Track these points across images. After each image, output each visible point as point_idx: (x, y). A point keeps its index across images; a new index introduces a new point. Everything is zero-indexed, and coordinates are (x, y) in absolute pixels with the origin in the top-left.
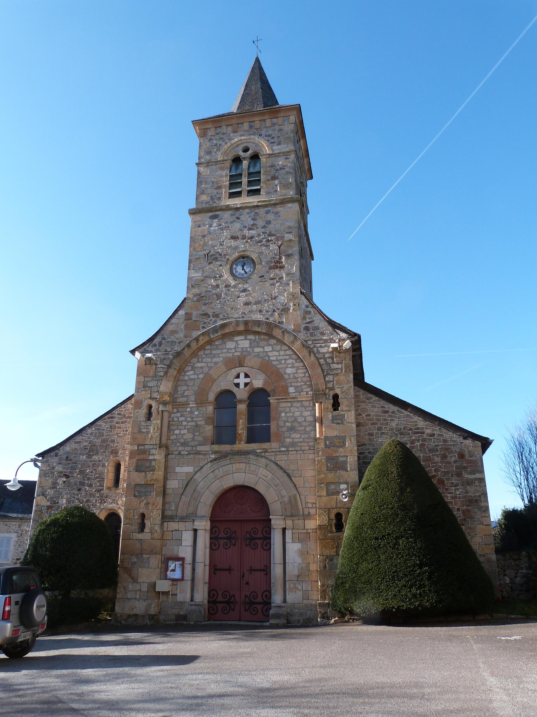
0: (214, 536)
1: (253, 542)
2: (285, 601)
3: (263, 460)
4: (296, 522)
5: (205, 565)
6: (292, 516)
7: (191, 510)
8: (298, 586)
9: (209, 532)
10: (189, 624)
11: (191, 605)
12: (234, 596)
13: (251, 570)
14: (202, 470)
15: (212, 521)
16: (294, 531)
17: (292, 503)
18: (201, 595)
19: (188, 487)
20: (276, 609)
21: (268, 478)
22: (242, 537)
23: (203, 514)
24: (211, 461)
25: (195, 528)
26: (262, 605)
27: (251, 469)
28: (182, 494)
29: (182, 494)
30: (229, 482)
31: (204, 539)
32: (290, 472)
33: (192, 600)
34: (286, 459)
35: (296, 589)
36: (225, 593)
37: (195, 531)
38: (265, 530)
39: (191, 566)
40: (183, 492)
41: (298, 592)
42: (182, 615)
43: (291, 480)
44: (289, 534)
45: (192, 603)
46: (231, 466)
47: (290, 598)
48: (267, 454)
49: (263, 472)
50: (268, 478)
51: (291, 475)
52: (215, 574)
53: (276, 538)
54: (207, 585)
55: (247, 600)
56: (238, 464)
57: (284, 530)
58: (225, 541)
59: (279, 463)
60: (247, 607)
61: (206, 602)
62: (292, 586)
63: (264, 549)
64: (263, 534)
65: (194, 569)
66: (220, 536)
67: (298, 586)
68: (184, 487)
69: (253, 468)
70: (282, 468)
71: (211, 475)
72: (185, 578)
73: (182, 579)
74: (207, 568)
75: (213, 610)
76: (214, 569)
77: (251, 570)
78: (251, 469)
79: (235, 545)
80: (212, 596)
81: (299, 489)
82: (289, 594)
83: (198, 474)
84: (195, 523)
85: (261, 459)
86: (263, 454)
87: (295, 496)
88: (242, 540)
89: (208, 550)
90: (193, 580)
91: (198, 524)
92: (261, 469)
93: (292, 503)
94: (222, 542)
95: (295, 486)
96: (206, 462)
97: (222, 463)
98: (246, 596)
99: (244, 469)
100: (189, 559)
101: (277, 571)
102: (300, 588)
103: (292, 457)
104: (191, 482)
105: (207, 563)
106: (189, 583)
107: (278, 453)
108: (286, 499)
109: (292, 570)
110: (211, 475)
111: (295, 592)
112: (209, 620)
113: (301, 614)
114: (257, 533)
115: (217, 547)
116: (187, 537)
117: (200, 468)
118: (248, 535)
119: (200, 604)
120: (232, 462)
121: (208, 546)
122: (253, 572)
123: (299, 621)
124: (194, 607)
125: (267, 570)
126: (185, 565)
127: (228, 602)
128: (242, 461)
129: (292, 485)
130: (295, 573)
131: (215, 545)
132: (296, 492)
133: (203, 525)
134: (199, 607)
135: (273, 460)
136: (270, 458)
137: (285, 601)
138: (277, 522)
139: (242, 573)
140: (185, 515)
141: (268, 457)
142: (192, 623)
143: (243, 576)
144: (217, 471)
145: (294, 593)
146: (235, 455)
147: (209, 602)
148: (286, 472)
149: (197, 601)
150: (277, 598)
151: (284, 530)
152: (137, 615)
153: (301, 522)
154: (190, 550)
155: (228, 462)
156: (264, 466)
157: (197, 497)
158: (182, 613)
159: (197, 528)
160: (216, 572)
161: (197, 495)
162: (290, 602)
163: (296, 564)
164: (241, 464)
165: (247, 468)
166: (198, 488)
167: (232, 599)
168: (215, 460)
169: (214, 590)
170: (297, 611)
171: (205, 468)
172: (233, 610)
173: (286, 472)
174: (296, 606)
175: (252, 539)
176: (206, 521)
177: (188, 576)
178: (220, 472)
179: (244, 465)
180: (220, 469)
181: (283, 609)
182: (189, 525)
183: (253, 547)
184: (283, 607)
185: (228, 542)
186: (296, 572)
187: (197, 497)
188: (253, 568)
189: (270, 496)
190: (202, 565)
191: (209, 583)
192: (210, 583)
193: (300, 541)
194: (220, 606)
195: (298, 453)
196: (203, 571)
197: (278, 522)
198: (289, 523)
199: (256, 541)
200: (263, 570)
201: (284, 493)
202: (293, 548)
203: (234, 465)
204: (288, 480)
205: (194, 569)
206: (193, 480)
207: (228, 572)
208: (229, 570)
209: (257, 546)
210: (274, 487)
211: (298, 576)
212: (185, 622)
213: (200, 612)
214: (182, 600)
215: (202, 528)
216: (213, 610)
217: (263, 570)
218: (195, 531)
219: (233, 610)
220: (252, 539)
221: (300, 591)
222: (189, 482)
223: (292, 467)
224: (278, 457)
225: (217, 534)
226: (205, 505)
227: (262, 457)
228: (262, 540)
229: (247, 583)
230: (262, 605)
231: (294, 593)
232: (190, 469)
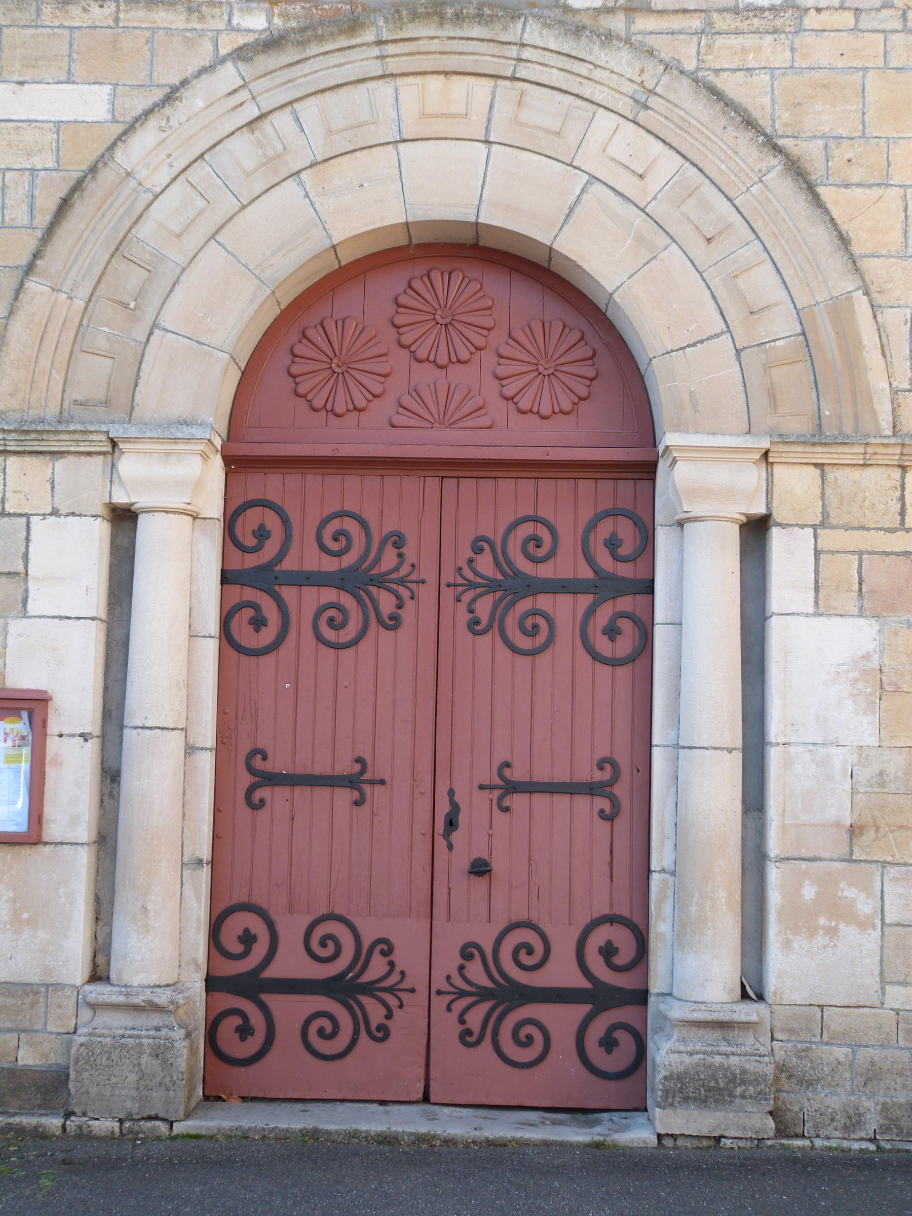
0: (251, 561)
1: (525, 605)
2: (751, 990)
3: (621, 61)
4: (843, 478)
5: (190, 750)
6: (818, 437)
7: (93, 377)
8: (850, 892)
9: (217, 531)
10: (84, 1136)
11: (94, 1007)
12: (387, 947)
13: (508, 787)
14: (178, 113)
15: (236, 464)
16: (830, 539)
17: (821, 352)
18: (165, 944)
19: (73, 223)
20: (701, 1041)
21: (654, 183)
22: (449, 576)
23: (179, 408)
24: (242, 54)
25: (120, 498)
26: (584, 1009)
27: (526, 115)
28: (30, 269)
29: (30, 269)
30: (370, 202)
31: (182, 575)
32: (810, 151)
33: (98, 975)
34: (782, 58)
35: (843, 912)
36: (330, 928)
37: (123, 518)
38: (605, 529)
39: (92, 748)
40: (37, 255)
41: (847, 931)
42: (26, 1071)
43: (817, 201)
44: (788, 554)
45: (99, 993)
46: (385, 89)
47: (790, 969)
48: (643, 23)
49: (611, 142)
50: (654, 183)
51: (816, 171)
52: (256, 806)
53: (696, 583)
54: (205, 874)
55: (476, 972)
56: (435, 82)
57: (756, 530)
58: (329, 595)
59: (729, 84)
60: (475, 1019)
61: (197, 985)
62: (809, 892)
63: (596, 657)
64: (589, 559)
65: (110, 776)
66: (289, 564)
67: (850, 892)
68: (43, 220)
69: (543, 108)
70: (749, 123)
71: (241, 145)
72: (53, 830)
73: (32, 836)
74: (206, 763)
75: (245, 1031)
76: (250, 777)
77: (508, 787)
78: (526, 115)
79: (394, 623)
80: (622, 1036)
81: (869, 265)
82: (787, 945)
83: (147, 137)
84: (127, 465)
85: (599, 54)
86: (617, 23)
87: (840, 310)
88: (448, 595)
89: (209, 649)
90: (106, 841)
91: (141, 475)
92: (605, 121)
93: (821, 352)
94: (306, 602)
95: (844, 241)
96: (205, 55)
97: (322, 67)
98: (468, 952)
99: (478, 118)
100: (76, 702)
101: (696, 792)
102: (865, 906)
103: (823, 51)
104: (95, 189)
105: (206, 734)
106: (82, 861)
107: (722, 22)
108: (781, 326)
109: (809, 791)
110: (242, 148)
111: (832, 932)
112: (212, 1098)
113: (872, 1076)
114: (552, 554)
115: (268, 635)
116: (69, 558)
117: (157, 95)
118: (485, 564)
119: (163, 998)
120: (393, 65)
121: (211, 623)
122: (518, 801)
123: (854, 1121)
124: (117, 1022)
125: (620, 789)
126: (53, 746)
127: (342, 988)
128: (467, 63)
129: (821, 236)
130: (831, 814)
131: (258, 623)
132: (848, 284)
133: (181, 487)
134: (156, 1019)
135: (690, 65)
136: (664, 47)
137: (751, 990)
138: (705, 473)
139: (443, 809)
140: (52, 410)
141: (651, 41)
142: (105, 1125)
143: (451, 824)
144: (283, 120)
145: (821, 939)
146: (415, 16)
147: (212, 983)
148: (776, 149)
149: (136, 981)
150: (694, 971)
151: (756, 530)
152: (646, 470)
153: (877, 482)
154: (85, 648)
155: (363, 62)
156: (624, 105)
157: (140, 295)
158: (27, 1058)
159: (140, 500)
160: (263, 793)
161: (134, 278)
162: (798, 997)
163: (840, 758)
164: (460, 84)
165: (504, 111)
166: (145, 231)
167: (377, 968)
168: (272, 43)
169: (331, 917)
170: (841, 1053)
171: (195, 99)
172: (382, 1034)
173: (776, 149)
174: (836, 1020)
175: (513, 586)
176: (205, 457)
177: (74, 820)
178: (307, 130)
179: (483, 86)
180: (309, 110)
181: (748, 1041)
182: (84, 480)
183: (524, 642)
184: (746, 1026)
185: (347, 601)
186: (839, 807)
187: (140, 295)
188: (518, 774)
189: (662, 307)
190: (176, 741)
191: (212, 862)
192: (218, 863)
193: (869, 602)
194: (290, 1011)
195: (866, 22)
196: (173, 789)
197: (719, 475)
198: (796, 484)
199: (544, 602)
200: (591, 789)
201: (763, 283)
202: (817, 651)
203: (409, 88)
204: (799, 203)
205: (110, 776)
206: (107, 175)
207: (344, 796)
208: (356, 781)
209: (551, 639)
210: (697, 249)
211: (854, 831)
212: (54, 1123)
213: (161, 1052)
214: (33, 976)
215: (177, 501)
216: (245, 1031)
217: (591, 789)
218: (123, 518)
219: (382, 1034)
220: (513, 586)
221: (864, 925)
222: (78, 187)
223: (824, 117)
224: (725, 52)
225: (271, 549)
226: (193, 370)
227: (608, 38)
228: (585, 601)
229: (480, 869)
230: (585, 1009)
231: (821, 939)
232: (89, 103)
